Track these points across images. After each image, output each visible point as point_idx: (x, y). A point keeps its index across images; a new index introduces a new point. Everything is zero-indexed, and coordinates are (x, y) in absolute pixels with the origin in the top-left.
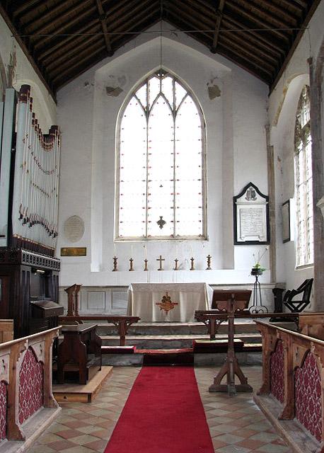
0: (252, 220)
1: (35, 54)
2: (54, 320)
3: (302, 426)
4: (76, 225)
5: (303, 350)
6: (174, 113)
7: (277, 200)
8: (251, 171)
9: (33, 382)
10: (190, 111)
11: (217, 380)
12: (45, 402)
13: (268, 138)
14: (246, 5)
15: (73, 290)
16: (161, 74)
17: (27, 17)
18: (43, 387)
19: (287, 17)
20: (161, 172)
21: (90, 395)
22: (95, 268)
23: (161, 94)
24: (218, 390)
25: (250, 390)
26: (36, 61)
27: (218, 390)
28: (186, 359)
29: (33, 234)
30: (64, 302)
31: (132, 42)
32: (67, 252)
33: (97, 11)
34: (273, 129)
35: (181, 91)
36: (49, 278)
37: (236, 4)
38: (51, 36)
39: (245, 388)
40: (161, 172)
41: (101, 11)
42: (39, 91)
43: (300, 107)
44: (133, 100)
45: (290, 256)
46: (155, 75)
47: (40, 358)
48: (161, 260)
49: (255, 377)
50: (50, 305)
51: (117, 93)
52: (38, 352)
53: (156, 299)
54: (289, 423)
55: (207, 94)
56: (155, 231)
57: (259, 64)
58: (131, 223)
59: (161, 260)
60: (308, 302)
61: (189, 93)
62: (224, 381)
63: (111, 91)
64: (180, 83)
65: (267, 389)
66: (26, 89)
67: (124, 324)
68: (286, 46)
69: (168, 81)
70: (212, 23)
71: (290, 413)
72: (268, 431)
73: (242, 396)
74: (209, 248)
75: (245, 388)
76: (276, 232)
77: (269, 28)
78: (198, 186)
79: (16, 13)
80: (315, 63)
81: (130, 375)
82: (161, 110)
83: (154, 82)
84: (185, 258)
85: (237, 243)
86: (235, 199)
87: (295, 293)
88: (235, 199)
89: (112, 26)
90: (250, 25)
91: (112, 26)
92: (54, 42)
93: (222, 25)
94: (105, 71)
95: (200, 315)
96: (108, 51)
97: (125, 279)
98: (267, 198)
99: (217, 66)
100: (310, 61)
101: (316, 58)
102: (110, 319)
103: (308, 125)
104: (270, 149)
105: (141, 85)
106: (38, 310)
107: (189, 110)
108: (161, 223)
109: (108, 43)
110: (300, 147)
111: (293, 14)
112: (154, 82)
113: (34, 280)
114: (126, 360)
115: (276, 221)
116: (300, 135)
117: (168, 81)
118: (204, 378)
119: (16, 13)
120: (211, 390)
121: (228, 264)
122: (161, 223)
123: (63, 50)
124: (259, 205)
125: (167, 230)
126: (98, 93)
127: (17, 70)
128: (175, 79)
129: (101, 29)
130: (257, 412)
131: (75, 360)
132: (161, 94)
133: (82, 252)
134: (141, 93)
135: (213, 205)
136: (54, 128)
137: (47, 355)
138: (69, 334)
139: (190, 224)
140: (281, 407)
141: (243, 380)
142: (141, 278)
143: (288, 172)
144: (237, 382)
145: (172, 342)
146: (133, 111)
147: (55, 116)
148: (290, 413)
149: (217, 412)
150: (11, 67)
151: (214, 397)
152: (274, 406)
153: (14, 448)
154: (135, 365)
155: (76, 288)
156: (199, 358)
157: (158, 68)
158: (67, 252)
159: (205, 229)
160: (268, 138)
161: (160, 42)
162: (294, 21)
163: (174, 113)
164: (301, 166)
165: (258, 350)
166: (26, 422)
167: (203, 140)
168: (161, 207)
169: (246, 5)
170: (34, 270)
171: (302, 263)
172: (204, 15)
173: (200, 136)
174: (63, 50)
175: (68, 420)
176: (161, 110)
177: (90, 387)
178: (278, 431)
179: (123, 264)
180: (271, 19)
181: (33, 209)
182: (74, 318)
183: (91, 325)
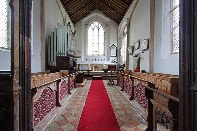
0: (114, 51)
1: (70, 15)
2: (76, 71)
3: (126, 92)
4: (79, 52)
5: (126, 77)
6: (99, 30)
7: (119, 48)
8: (114, 42)
9: (73, 83)
10: (102, 30)
11: (109, 82)
12: (75, 87)
13: (117, 35)
14: (116, 1)
15: (79, 65)
16: (96, 21)
17: (70, 9)
18: (75, 84)
19: (123, 9)
20: (96, 42)
21: (83, 85)
22: (83, 61)
23: (96, 26)
24: (108, 84)
25: (115, 85)
26: (65, 6)
27: (108, 84)
28: (101, 78)
29: (72, 54)
30: (77, 67)
31: (90, 14)
32: (78, 57)
33: (83, 6)
34: (119, 33)
35: (100, 25)
36: (75, 63)
37: (114, 1)
38: (73, 12)
39: (114, 84)
40: (96, 42)
41: (84, 7)
42: (71, 24)
43: (125, 29)
44: (90, 27)
45: (121, 59)
46: (95, 21)
47: (74, 78)
48: (96, 59)
49: (115, 81)
50: (74, 68)
51: (87, 25)
52: (73, 77)
53: (94, 67)
54: (123, 91)
55: (106, 26)
56: (95, 53)
57: (116, 19)
58: (90, 52)
59: (96, 59)
60: (124, 68)
61: (102, 25)
62: (110, 83)
63: (86, 25)
64: (100, 23)
65: (117, 85)
66: (69, 23)
67: (89, 72)
68: (123, 15)
69: (97, 23)
70: (107, 10)
71: (123, 90)
72: (118, 93)
73: (113, 86)
74: (105, 57)
75: (114, 84)
76: (118, 54)
77: (119, 11)
78: (103, 45)
79: (66, 6)
80: (129, 19)
81: (91, 81)
82: (96, 29)
83: (95, 23)
84: (100, 59)
85: (110, 56)
86: (110, 47)
87: (121, 66)
88: (110, 47)
89: (86, 10)
90: (115, 10)
91: (86, 10)
92: (73, 14)
93: (109, 12)
94: (85, 20)
95: (103, 70)
96: (85, 15)
97: (89, 63)
98: (117, 47)
99: (107, 19)
100: (128, 18)
101: (129, 18)
102: (86, 70)
103: (126, 33)
104: (118, 37)
105: (92, 23)
106: (73, 69)
107: (102, 30)
108: (96, 52)
109: (85, 14)
110: (124, 37)
111: (125, 8)
112: (95, 23)
113: (72, 63)
114: (90, 78)
115: (118, 52)
116: (124, 35)
117: (97, 23)
118: (105, 82)
119: (66, 6)
120: (107, 84)
121: (108, 60)
122: (96, 52)
123: (76, 15)
124: (115, 49)
125: (97, 54)
126: (83, 25)
127: (66, 19)
128: (99, 22)
129: (84, 11)
130: (115, 89)
131: (80, 78)
132: (96, 26)
133: (80, 57)
134: (92, 25)
135: (106, 48)
136: (75, 32)
137: (75, 77)
138: (79, 73)
139: (101, 52)
140: (121, 89)
141: (114, 83)
142: (92, 63)
143: (121, 42)
144: (112, 83)
145: (98, 75)
146: (90, 29)
147: (75, 30)
148: (123, 90)
149: (109, 89)
150: (65, 18)
151: (108, 86)
152: (119, 88)
153: (70, 96)
154: (91, 79)
155: (79, 64)
156: (103, 78)
157: (96, 20)
158: (78, 57)
159: (104, 53)
160: (117, 35)
161: (96, 14)
162: (125, 10)
163: (99, 30)
164: (124, 41)
165: (116, 77)
166: (71, 91)
167: (104, 35)
168: (96, 49)
169: (116, 1)
170: (72, 61)
171: (123, 60)
172: (105, 8)
173: (103, 35)
174: (76, 15)
175: (78, 92)
176: (96, 29)
177: (83, 84)
178: (120, 93)
179: (88, 60)
180: (119, 9)
181: (72, 49)
182: (79, 70)
183: (83, 71)
